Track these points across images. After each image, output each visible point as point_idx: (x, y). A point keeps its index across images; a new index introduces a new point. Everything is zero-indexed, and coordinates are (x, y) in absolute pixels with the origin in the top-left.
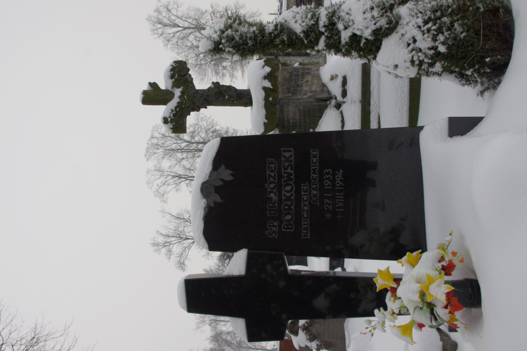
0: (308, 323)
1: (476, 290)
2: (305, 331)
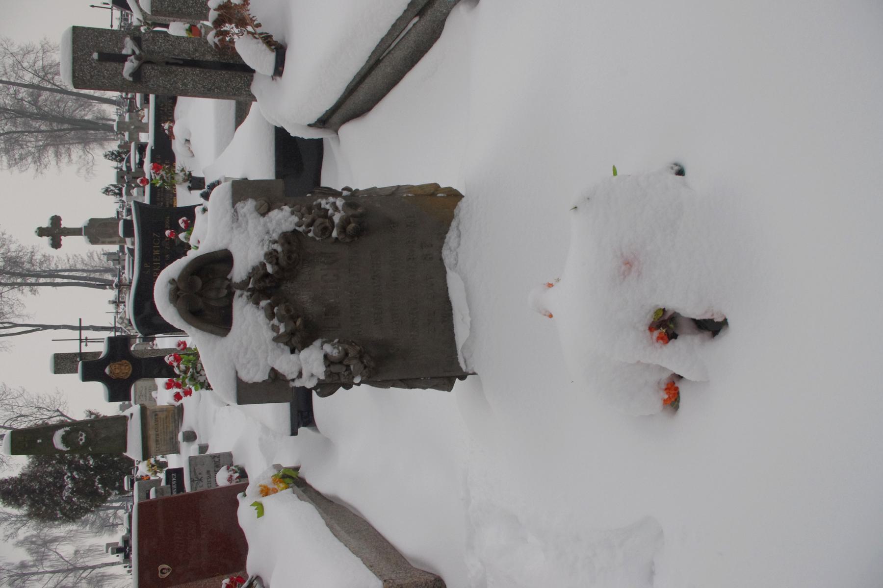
0: (277, 259)
2: (263, 303)
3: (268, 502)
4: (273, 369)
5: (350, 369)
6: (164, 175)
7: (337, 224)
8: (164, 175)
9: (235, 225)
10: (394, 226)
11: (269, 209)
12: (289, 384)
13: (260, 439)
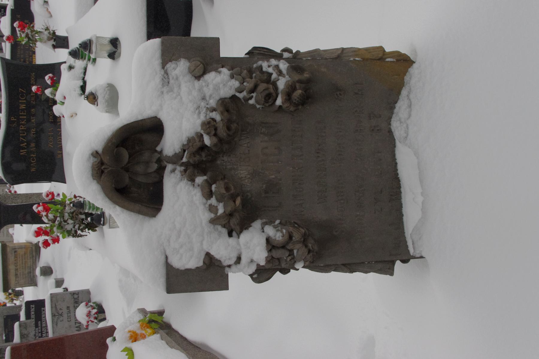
0: (216, 129)
1: (51, 146)
2: (200, 180)
3: (138, 347)
4: (208, 254)
5: (293, 254)
6: (30, 33)
7: (282, 90)
8: (30, 33)
9: (165, 89)
10: (340, 94)
11: (205, 72)
12: (224, 270)
13: (120, 281)
